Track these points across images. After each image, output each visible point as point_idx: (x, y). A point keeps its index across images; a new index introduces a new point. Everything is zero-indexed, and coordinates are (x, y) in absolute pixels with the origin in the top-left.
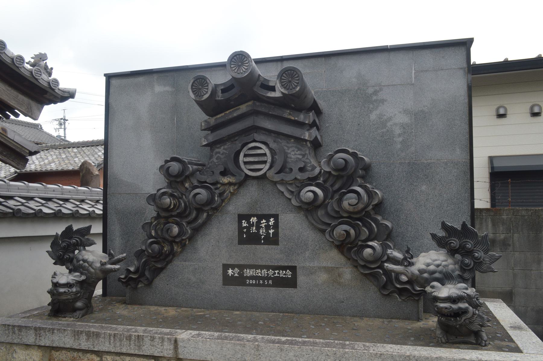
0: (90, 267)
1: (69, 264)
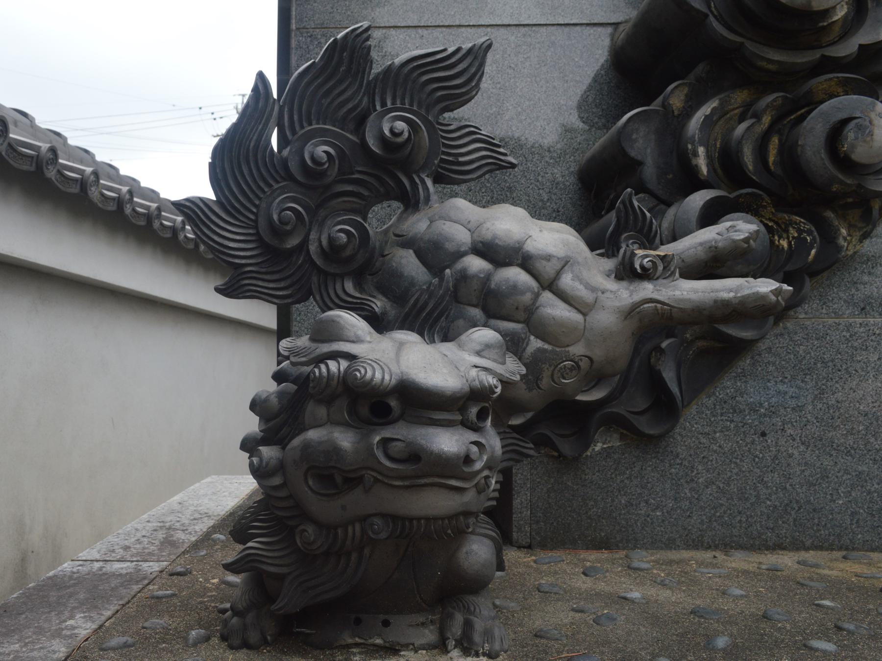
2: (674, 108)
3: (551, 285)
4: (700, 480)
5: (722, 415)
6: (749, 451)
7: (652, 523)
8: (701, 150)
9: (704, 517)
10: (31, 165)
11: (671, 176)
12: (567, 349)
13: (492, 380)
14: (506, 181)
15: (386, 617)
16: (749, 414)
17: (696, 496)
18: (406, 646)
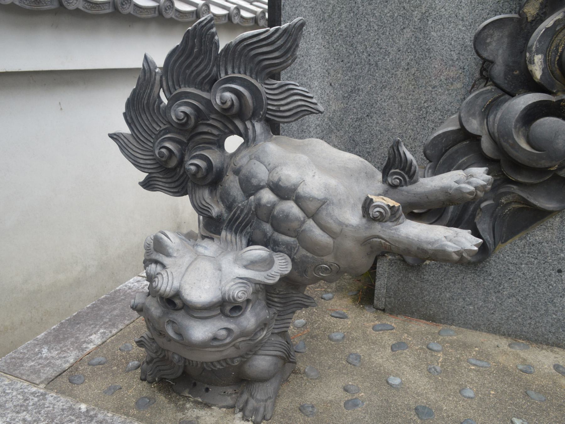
0: (310, 223)
1: (206, 194)
2: (528, 15)
3: (313, 216)
4: (505, 293)
5: (529, 254)
6: (546, 280)
7: (466, 312)
8: (538, 58)
9: (504, 316)
10: (155, 13)
11: (518, 72)
12: (322, 258)
13: (430, 171)
14: (426, 44)
15: (208, 386)
16: (551, 256)
17: (500, 302)
18: (215, 405)
